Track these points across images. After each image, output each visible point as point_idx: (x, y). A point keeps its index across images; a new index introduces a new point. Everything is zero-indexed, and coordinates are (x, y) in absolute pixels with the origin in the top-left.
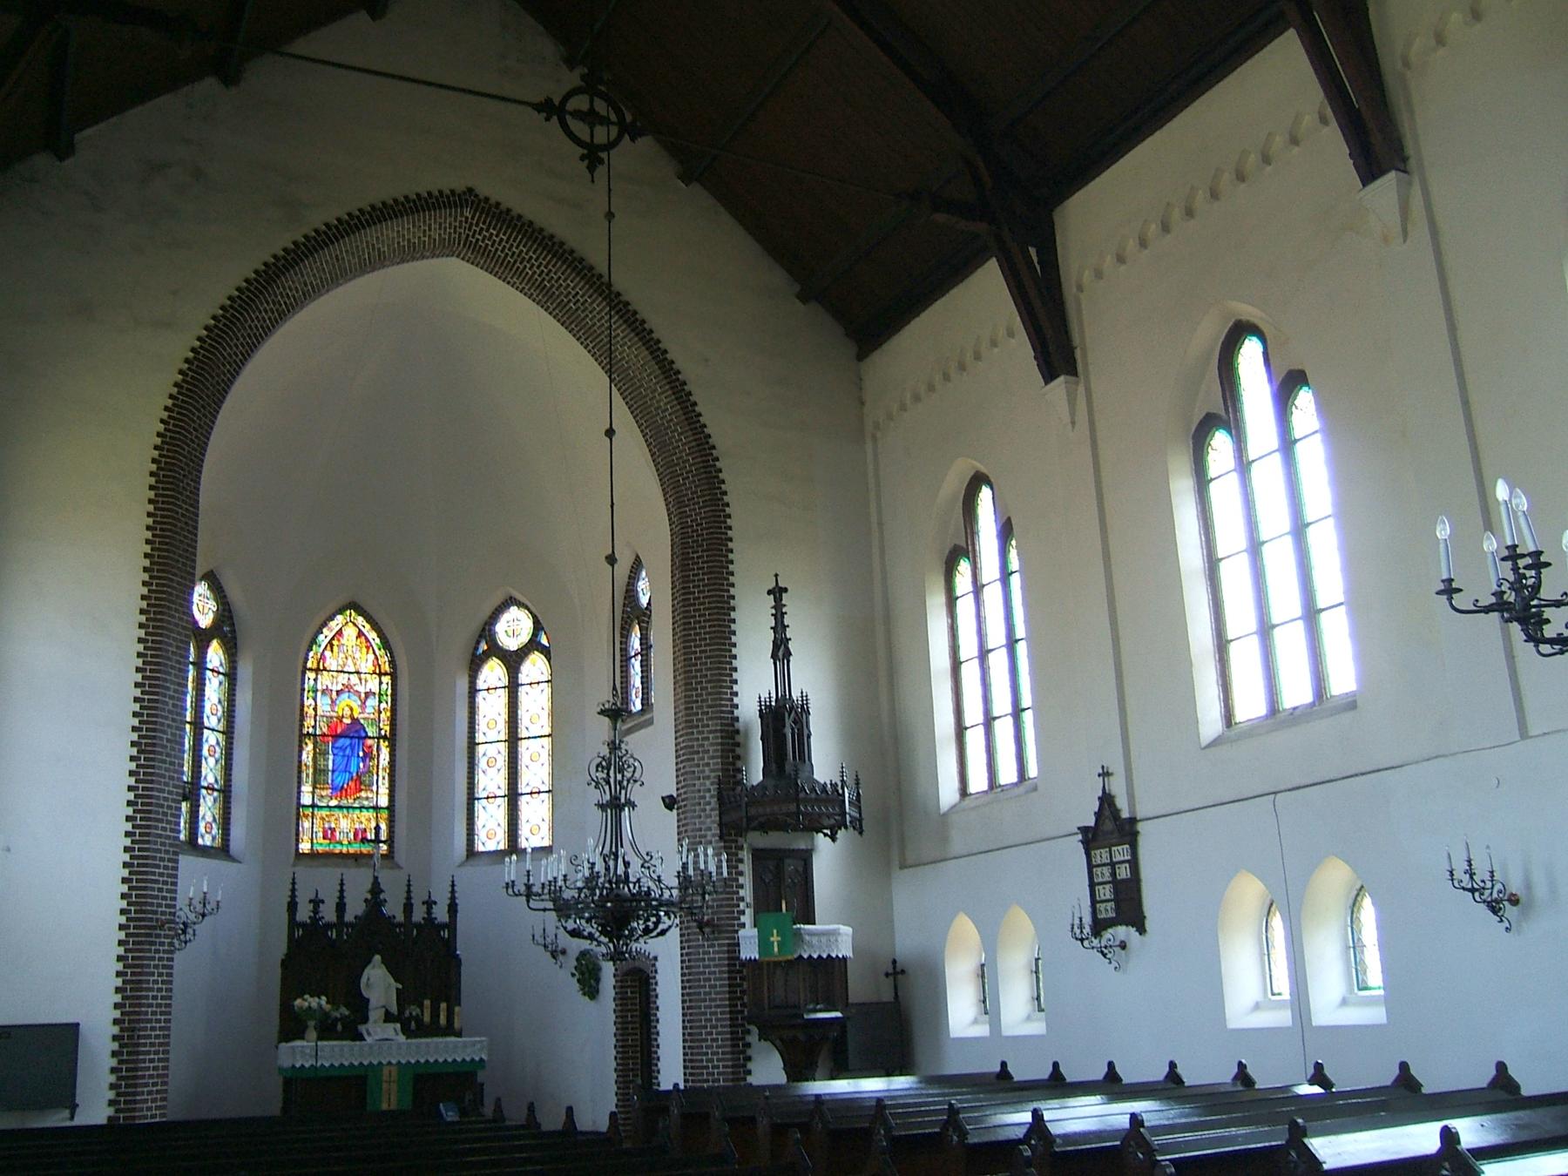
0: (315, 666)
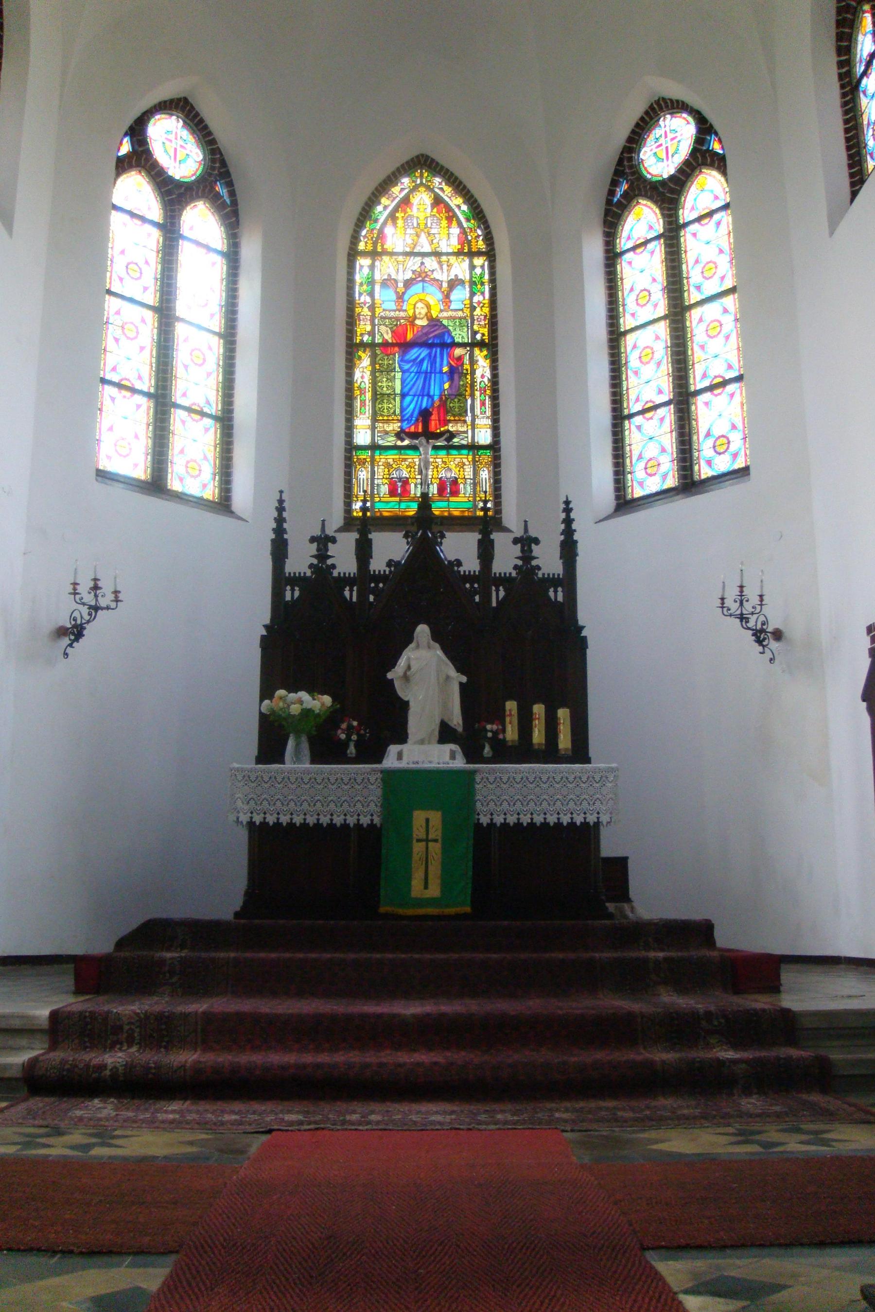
0: (370, 248)
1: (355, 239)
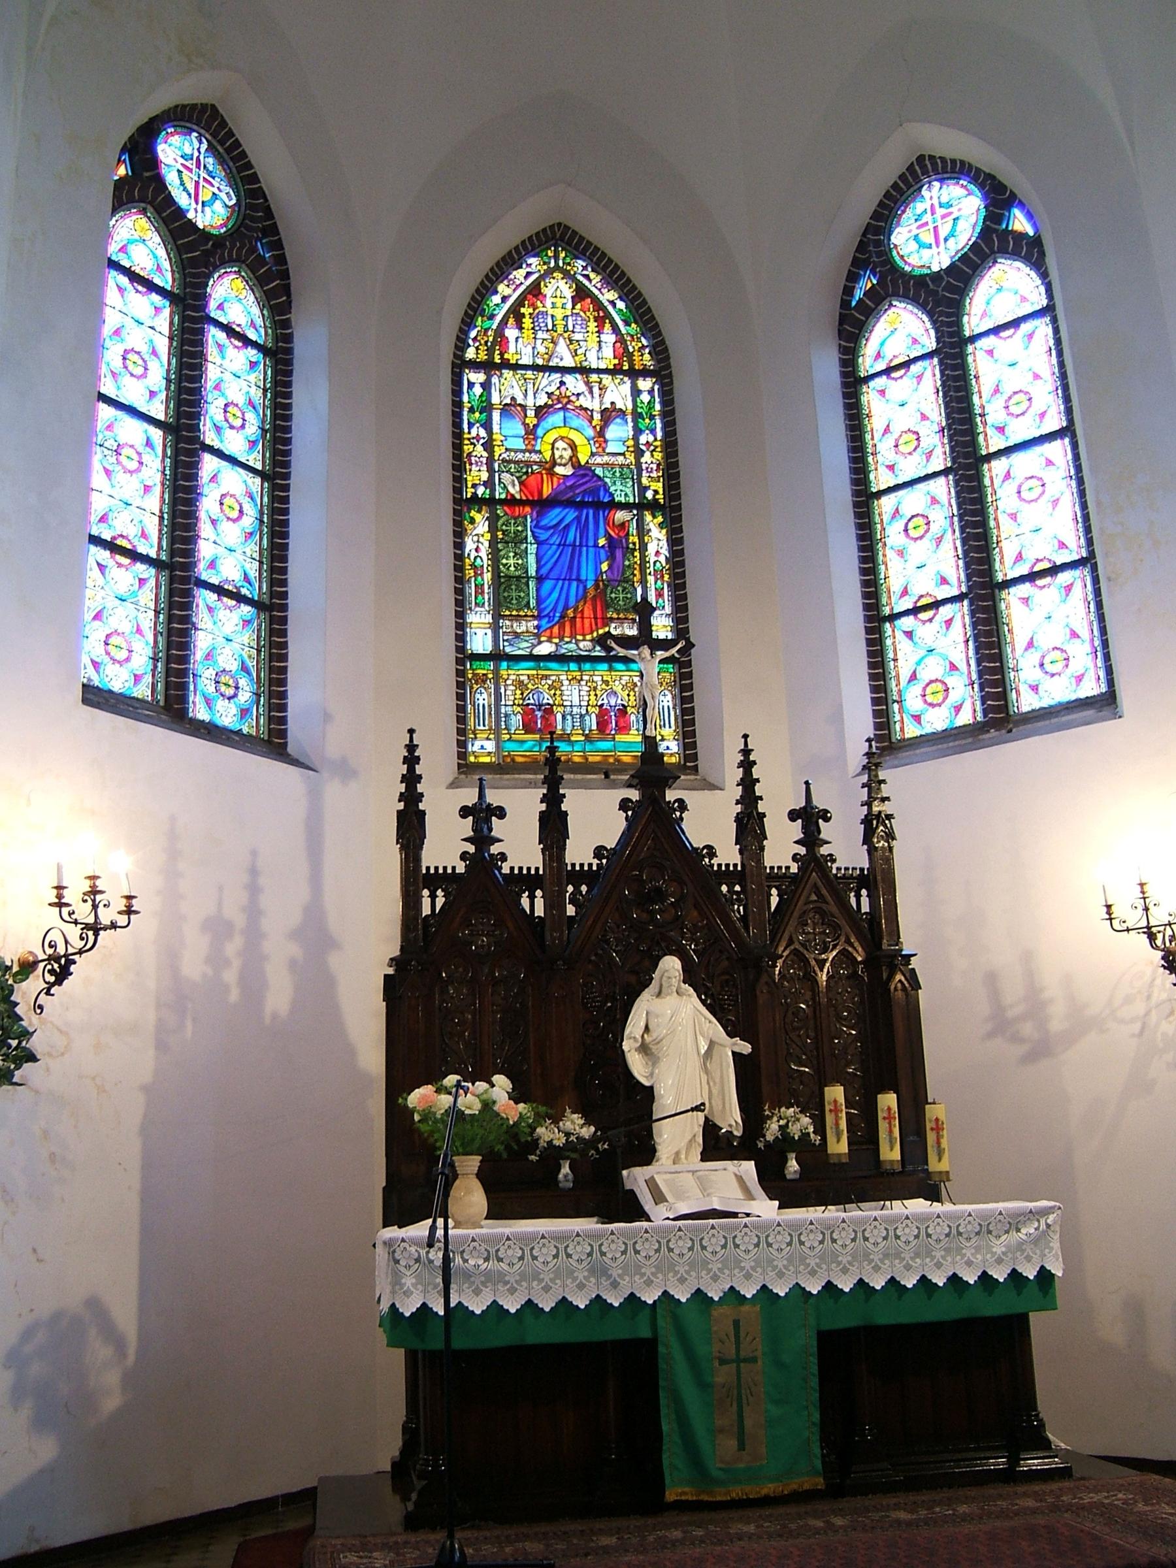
0: (483, 356)
1: (461, 344)
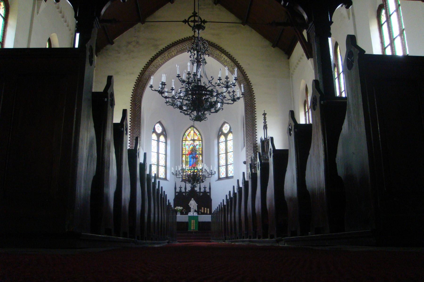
0: (185, 140)
1: (183, 138)
